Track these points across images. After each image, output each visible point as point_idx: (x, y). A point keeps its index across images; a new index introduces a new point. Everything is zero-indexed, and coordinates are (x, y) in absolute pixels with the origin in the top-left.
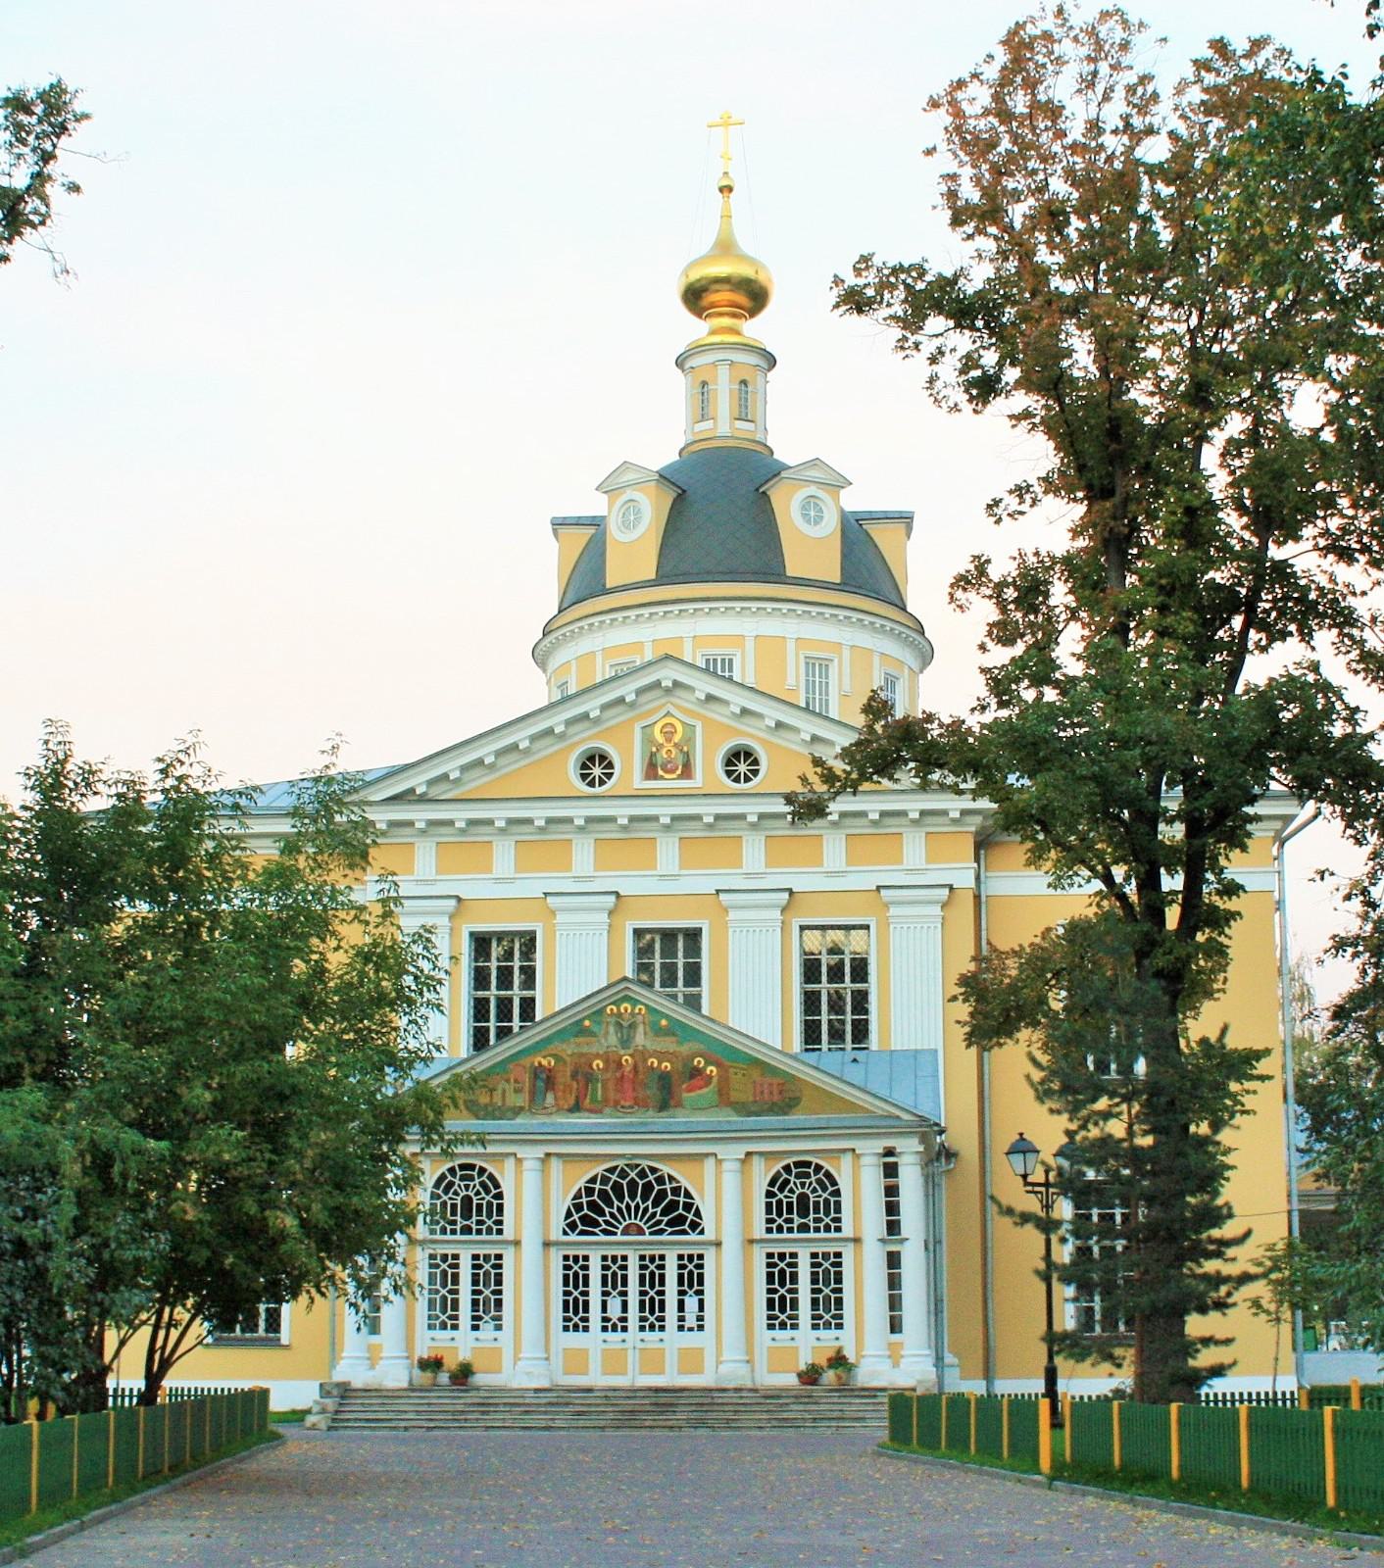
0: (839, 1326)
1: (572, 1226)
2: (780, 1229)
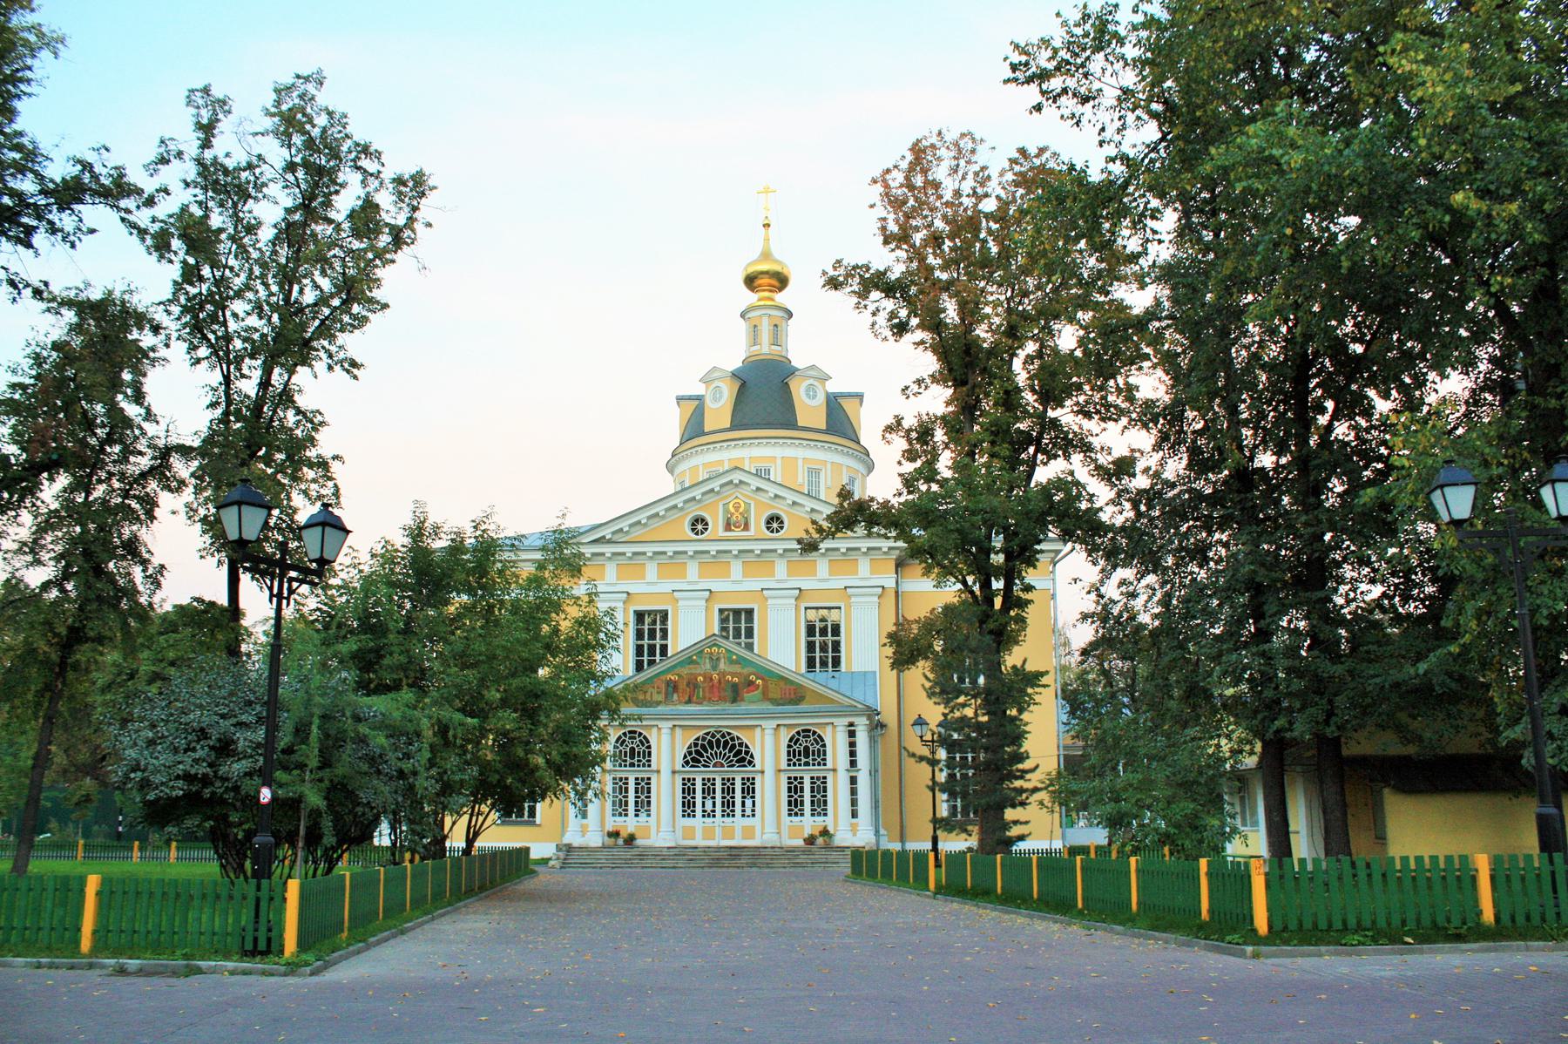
0: (825, 815)
1: (687, 763)
2: (794, 764)
